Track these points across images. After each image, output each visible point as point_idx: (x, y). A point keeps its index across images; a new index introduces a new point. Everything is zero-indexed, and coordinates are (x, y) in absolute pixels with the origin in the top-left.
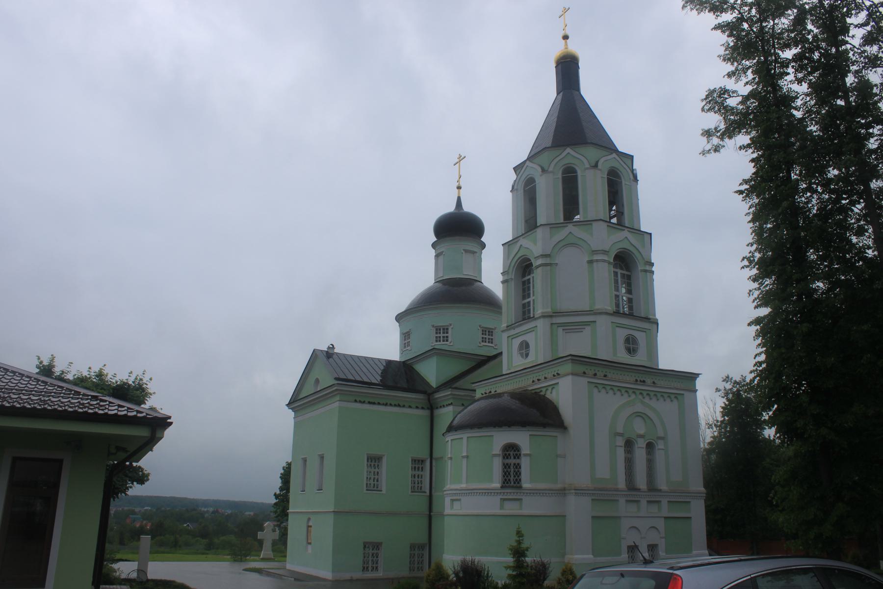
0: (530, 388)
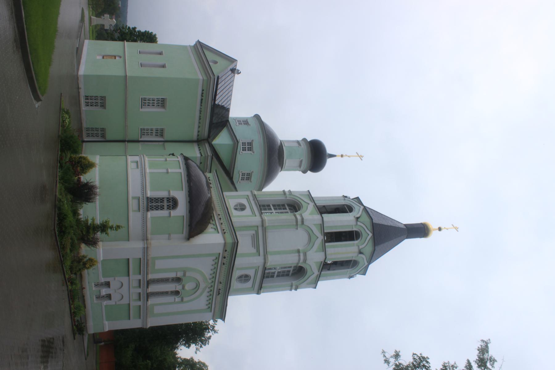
0: (214, 212)
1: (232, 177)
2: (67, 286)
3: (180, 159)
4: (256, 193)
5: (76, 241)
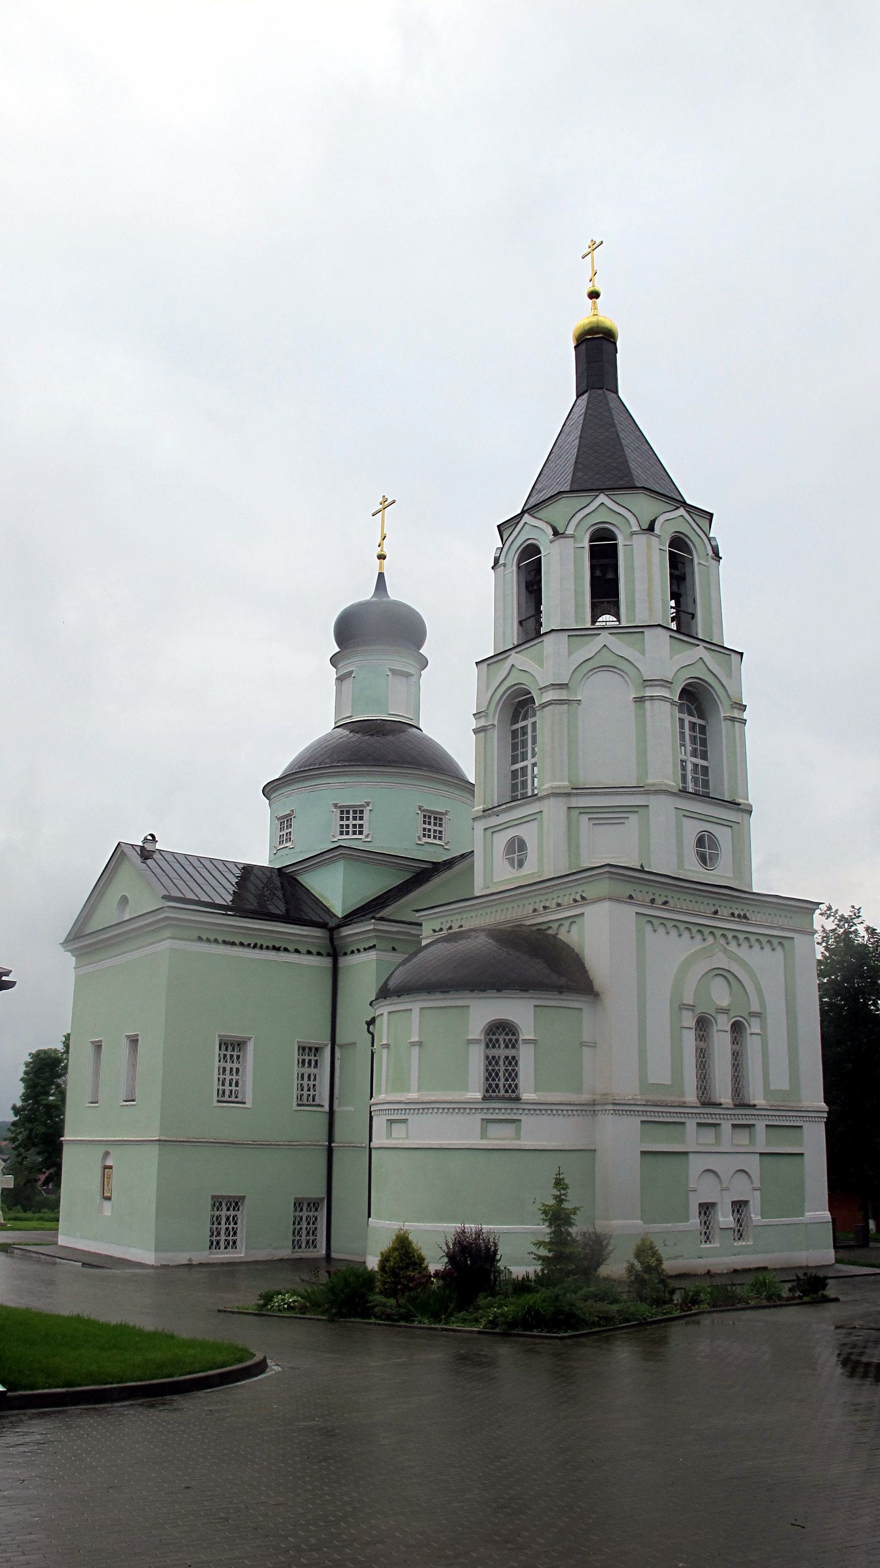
2: (703, 1313)
3: (384, 1009)
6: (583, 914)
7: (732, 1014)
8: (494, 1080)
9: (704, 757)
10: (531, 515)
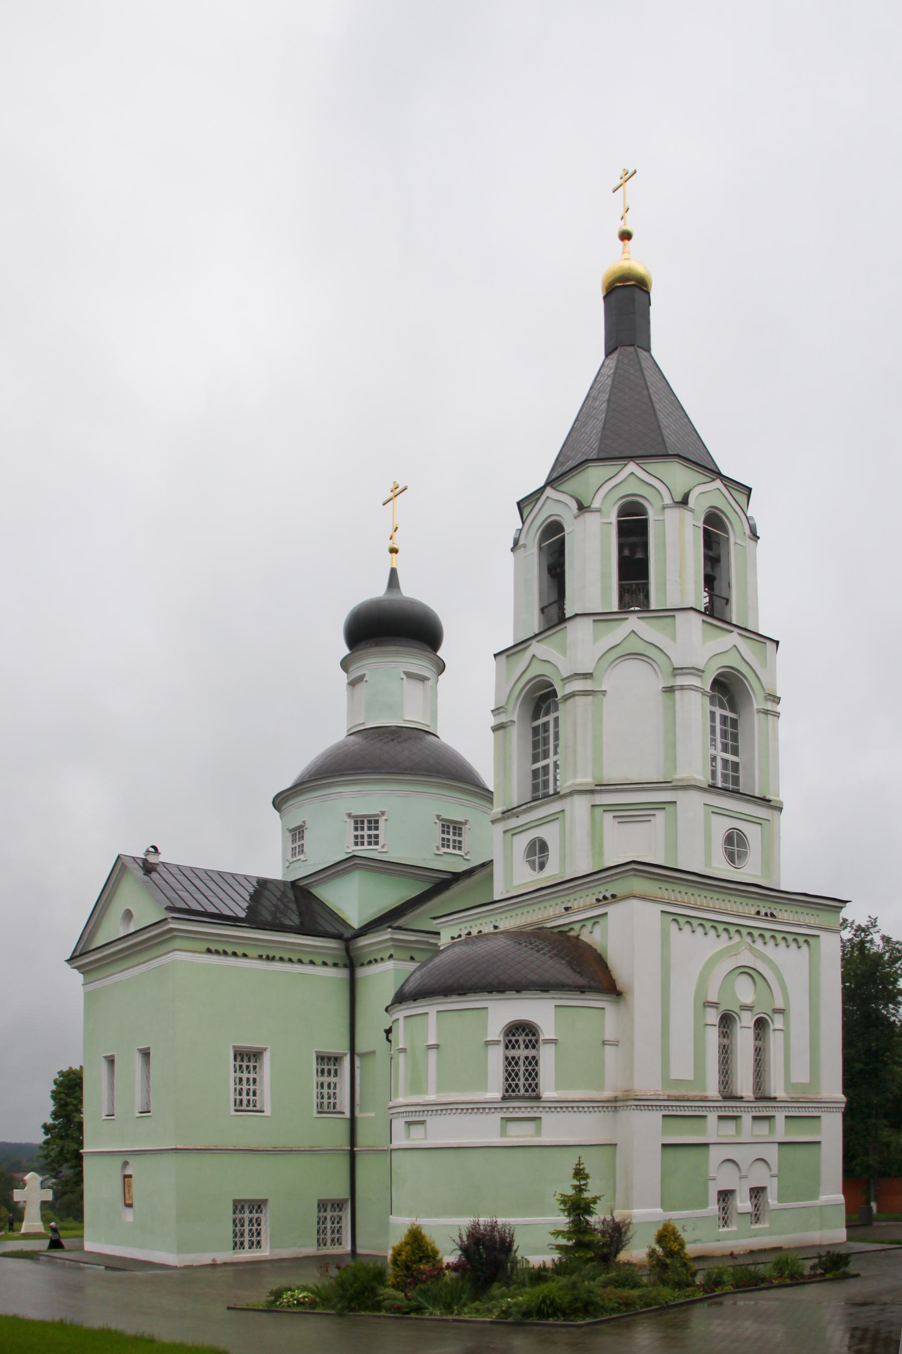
1: (453, 873)
3: (401, 1013)
4: (497, 809)
5: (612, 1274)
6: (606, 914)
7: (756, 1010)
8: (513, 1080)
9: (735, 752)
10: (554, 489)
